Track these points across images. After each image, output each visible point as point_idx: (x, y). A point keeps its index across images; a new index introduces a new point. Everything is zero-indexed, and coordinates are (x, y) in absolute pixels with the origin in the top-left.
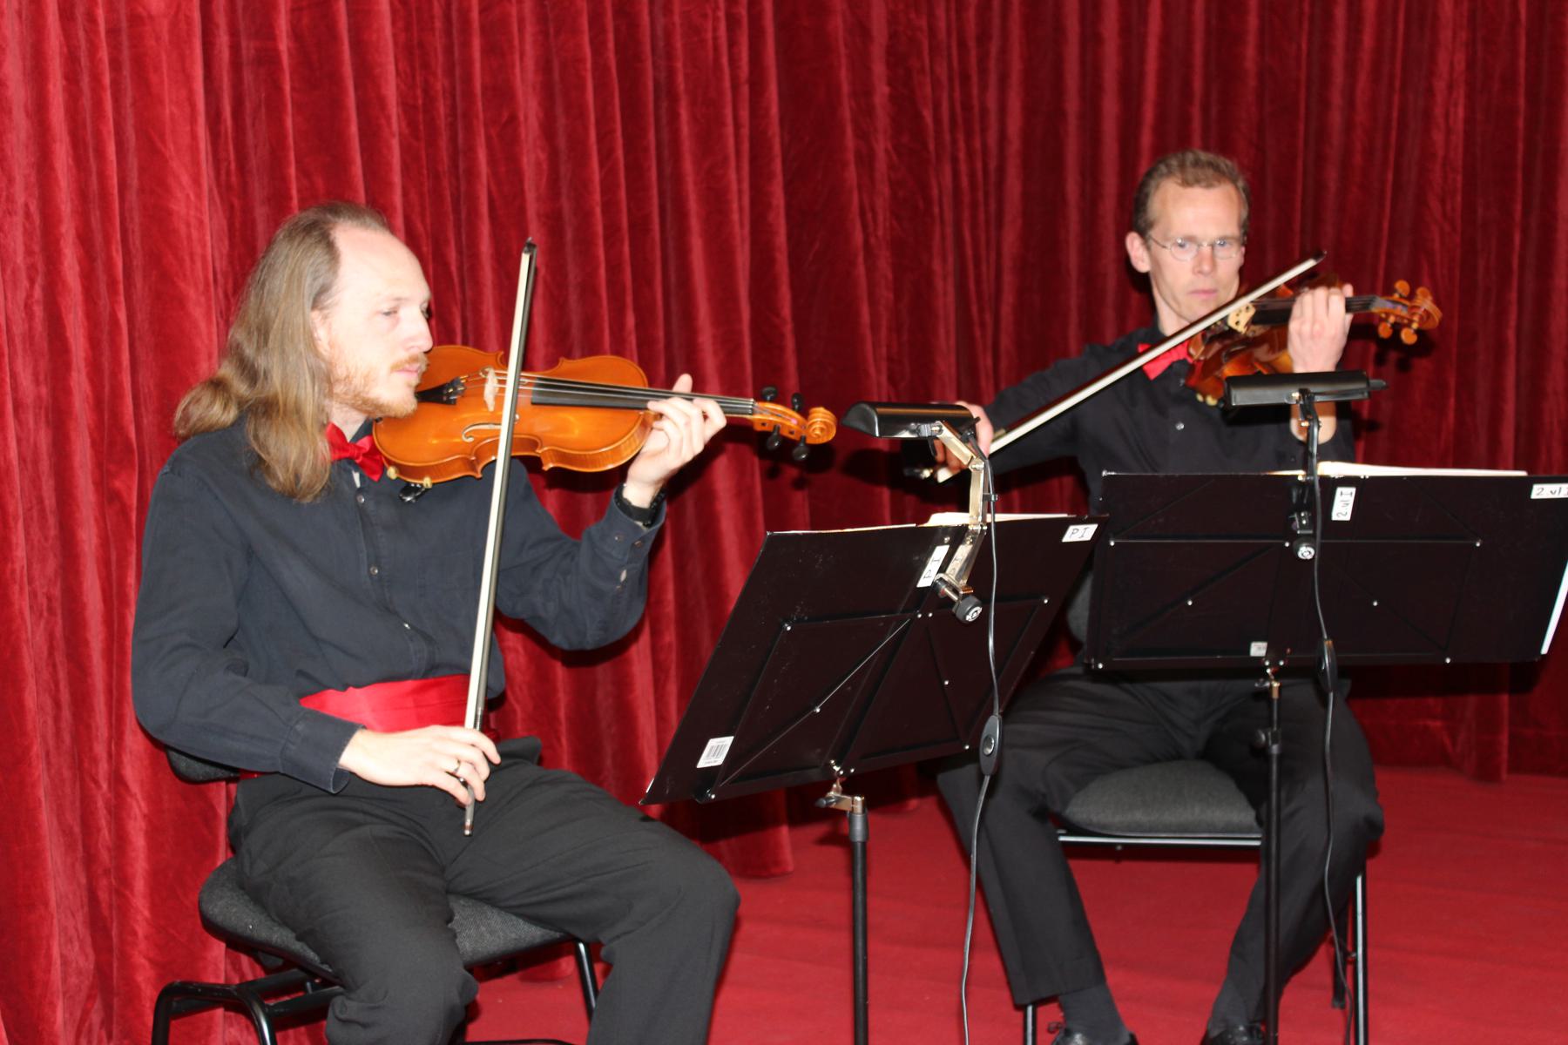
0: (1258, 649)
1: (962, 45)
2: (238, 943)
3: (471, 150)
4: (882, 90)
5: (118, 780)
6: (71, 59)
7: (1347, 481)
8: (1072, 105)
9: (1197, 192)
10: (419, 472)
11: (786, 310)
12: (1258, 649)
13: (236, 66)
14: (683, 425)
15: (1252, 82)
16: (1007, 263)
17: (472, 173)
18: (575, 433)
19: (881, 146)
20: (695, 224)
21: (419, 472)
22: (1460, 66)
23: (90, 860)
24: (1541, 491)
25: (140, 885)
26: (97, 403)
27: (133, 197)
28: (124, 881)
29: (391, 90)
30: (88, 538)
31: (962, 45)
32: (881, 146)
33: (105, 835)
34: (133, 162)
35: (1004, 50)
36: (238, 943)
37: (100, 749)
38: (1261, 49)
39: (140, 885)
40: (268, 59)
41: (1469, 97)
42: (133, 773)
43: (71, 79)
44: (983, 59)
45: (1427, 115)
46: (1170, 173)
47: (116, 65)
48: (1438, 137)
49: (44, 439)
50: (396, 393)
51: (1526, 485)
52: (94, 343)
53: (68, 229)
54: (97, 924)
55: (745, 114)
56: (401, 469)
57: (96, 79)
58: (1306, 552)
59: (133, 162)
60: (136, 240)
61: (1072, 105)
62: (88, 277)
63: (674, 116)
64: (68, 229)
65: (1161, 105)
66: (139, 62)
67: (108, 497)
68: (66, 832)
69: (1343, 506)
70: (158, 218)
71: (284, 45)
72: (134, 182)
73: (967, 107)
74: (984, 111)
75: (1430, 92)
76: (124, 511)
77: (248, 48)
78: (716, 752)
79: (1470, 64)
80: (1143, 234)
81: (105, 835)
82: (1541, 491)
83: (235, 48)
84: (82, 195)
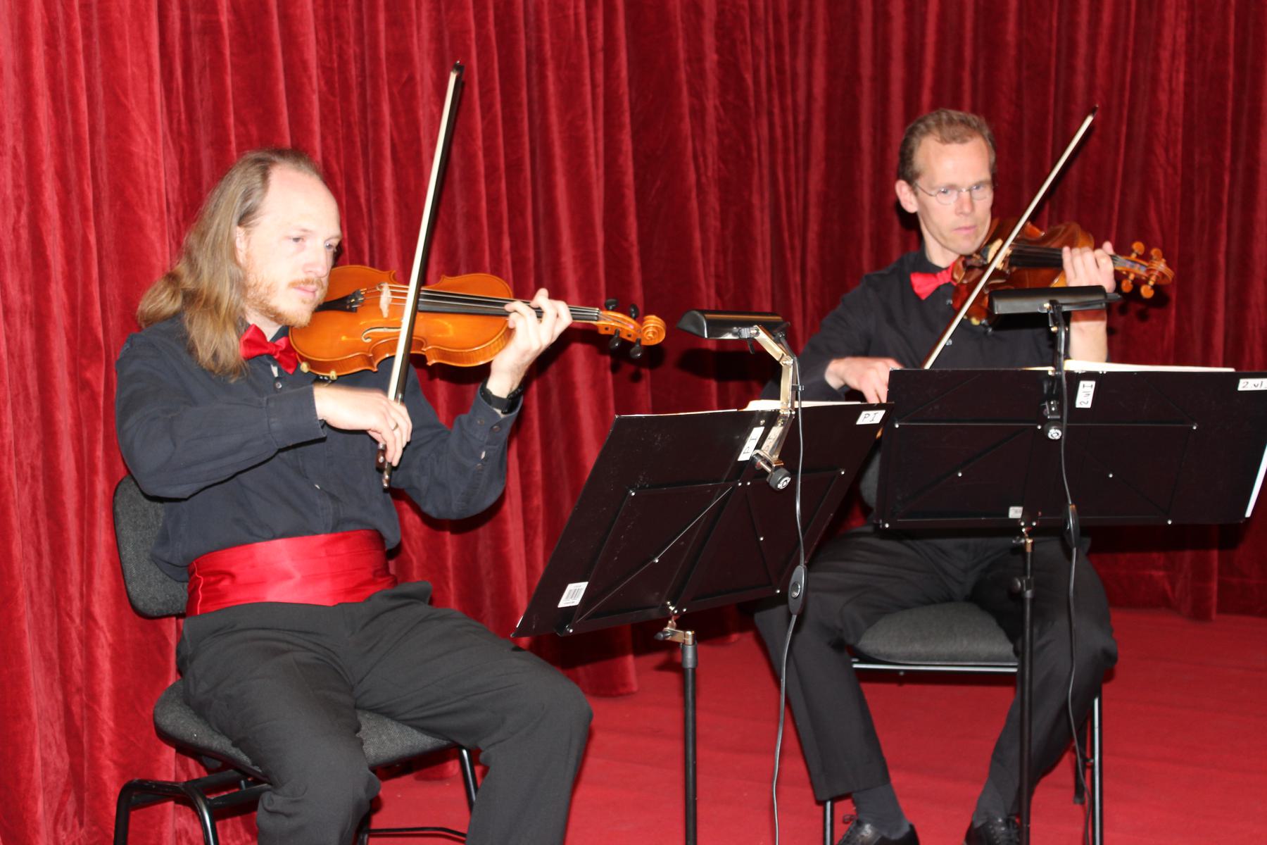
0: (1015, 512)
1: (777, 21)
2: (185, 749)
3: (377, 103)
4: (711, 58)
5: (88, 615)
6: (51, 29)
7: (1088, 376)
8: (866, 70)
9: (954, 147)
10: (327, 366)
11: (633, 236)
12: (1015, 512)
13: (186, 34)
14: (537, 324)
15: (1012, 52)
16: (813, 199)
17: (377, 123)
18: (451, 334)
19: (711, 102)
20: (559, 165)
21: (327, 366)
22: (1181, 39)
23: (65, 681)
24: (1246, 385)
25: (106, 701)
26: (72, 310)
27: (101, 142)
28: (93, 697)
29: (312, 55)
30: (64, 418)
31: (777, 21)
32: (711, 102)
33: (78, 660)
34: (101, 113)
35: (811, 25)
36: (185, 749)
37: (74, 590)
38: (1019, 24)
39: (106, 701)
40: (211, 29)
41: (1189, 64)
42: (100, 610)
43: (51, 44)
44: (794, 32)
45: (1155, 79)
46: (928, 130)
47: (87, 33)
48: (1163, 97)
49: (28, 338)
50: (297, 307)
51: (1234, 379)
52: (69, 260)
53: (48, 168)
54: (71, 733)
55: (600, 77)
56: (312, 364)
57: (71, 44)
58: (1054, 433)
59: (101, 113)
60: (104, 177)
61: (866, 70)
62: (64, 206)
63: (542, 77)
64: (48, 168)
65: (938, 70)
66: (106, 31)
67: (81, 385)
68: (46, 658)
69: (1085, 396)
70: (122, 159)
71: (225, 18)
72: (102, 127)
73: (781, 71)
74: (795, 74)
75: (1157, 60)
76: (93, 397)
77: (196, 20)
78: (573, 594)
79: (1190, 38)
80: (911, 180)
81: (78, 660)
82: (1246, 385)
83: (185, 20)
84: (60, 139)
